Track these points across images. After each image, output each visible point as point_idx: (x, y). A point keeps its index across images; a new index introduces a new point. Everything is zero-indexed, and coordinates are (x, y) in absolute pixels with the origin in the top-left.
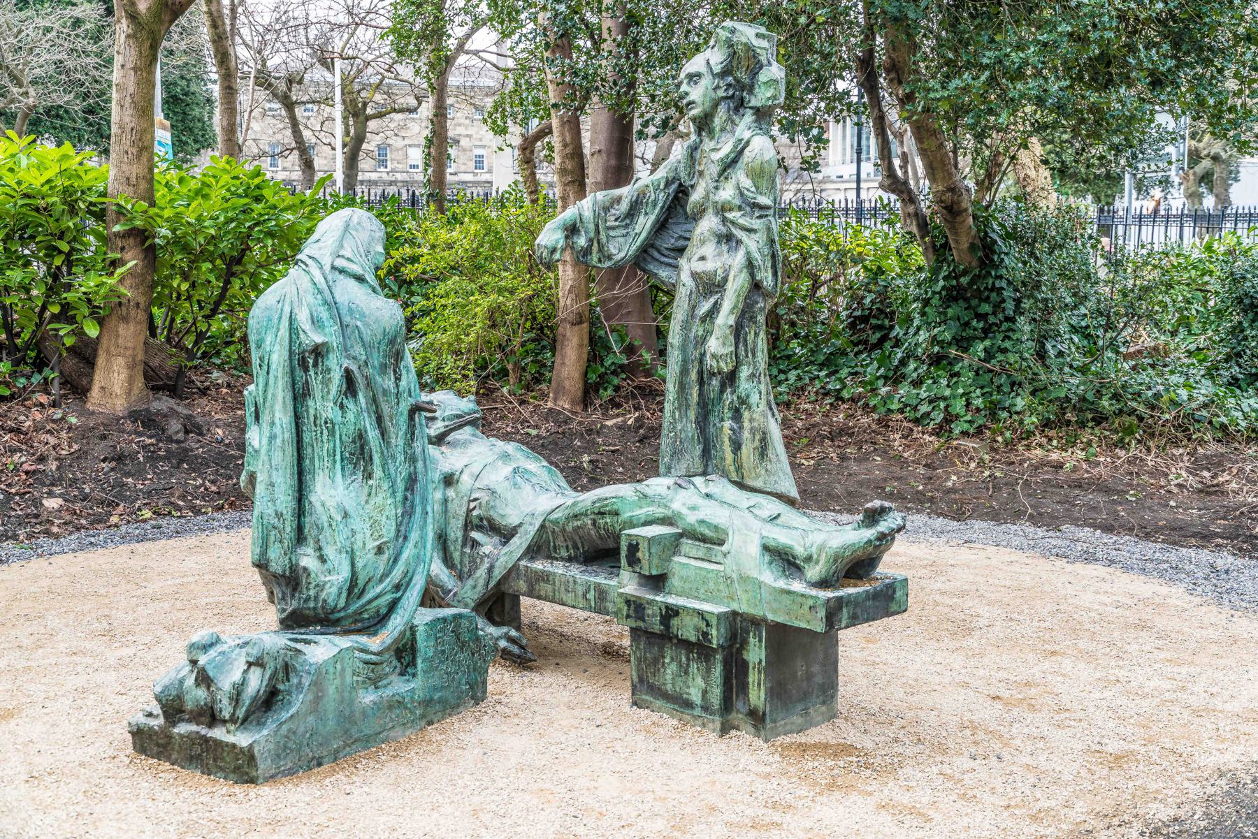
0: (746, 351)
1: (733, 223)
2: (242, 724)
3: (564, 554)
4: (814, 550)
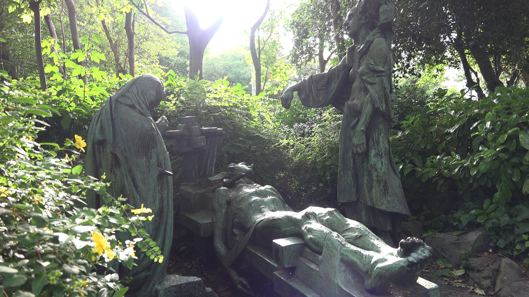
0: (373, 143)
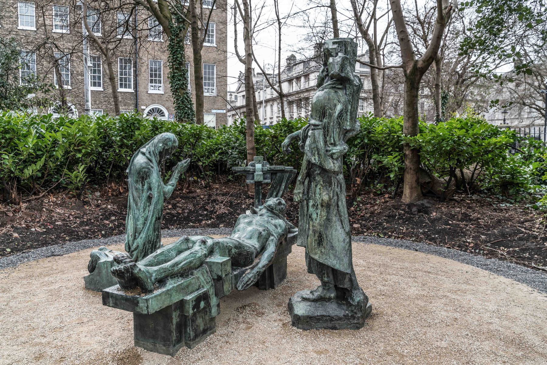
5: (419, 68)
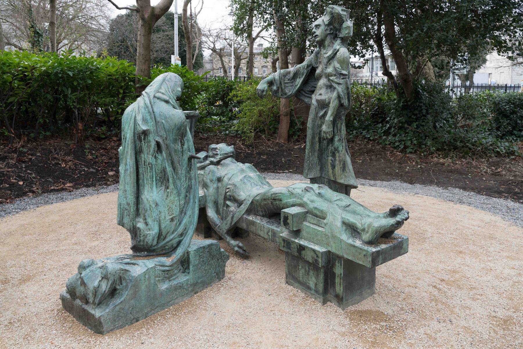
0: (337, 130)
1: (332, 81)
2: (98, 305)
3: (261, 214)
4: (366, 226)
5: (156, 15)
